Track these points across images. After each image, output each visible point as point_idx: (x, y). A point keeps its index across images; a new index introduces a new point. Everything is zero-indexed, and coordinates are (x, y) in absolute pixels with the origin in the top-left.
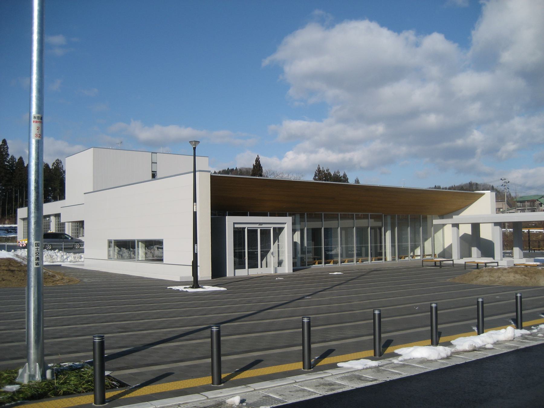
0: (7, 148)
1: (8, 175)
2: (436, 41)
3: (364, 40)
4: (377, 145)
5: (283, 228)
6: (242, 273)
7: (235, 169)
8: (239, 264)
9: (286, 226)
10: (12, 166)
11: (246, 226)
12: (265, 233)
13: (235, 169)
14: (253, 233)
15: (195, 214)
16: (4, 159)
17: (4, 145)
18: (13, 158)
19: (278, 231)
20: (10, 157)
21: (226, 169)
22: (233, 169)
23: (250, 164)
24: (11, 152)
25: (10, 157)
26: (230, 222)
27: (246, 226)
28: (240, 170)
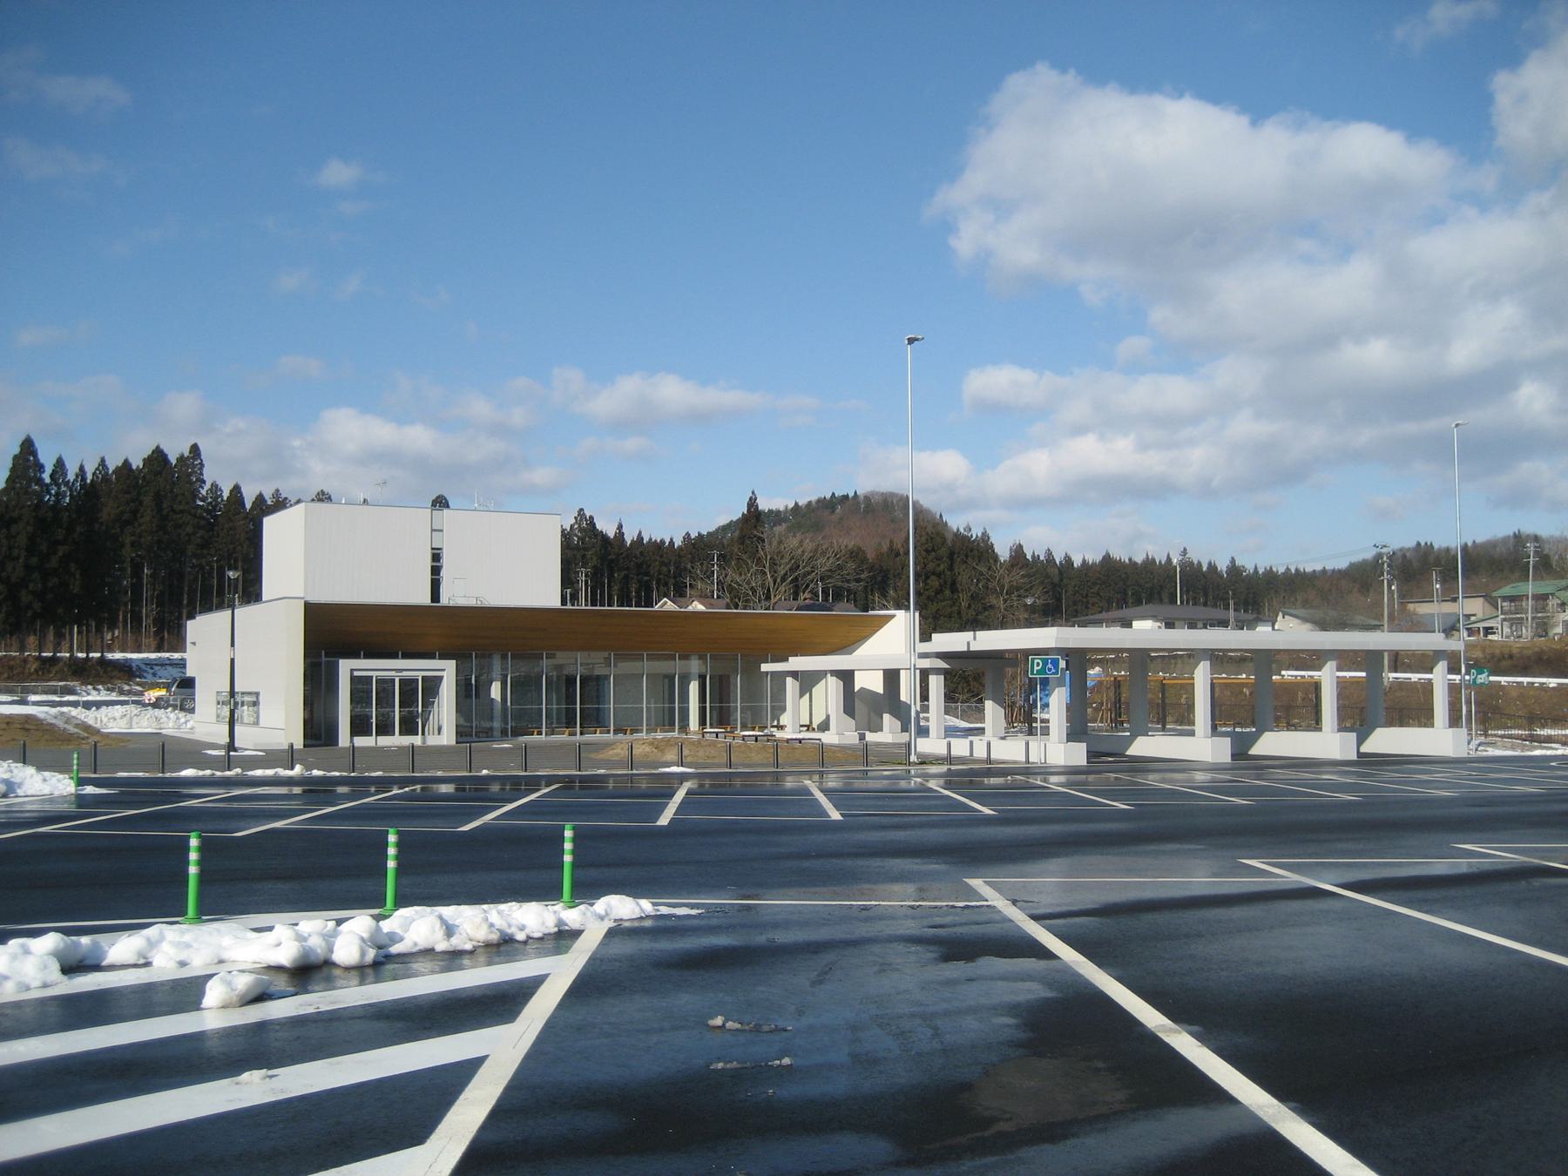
0: (202, 465)
1: (201, 533)
2: (1366, 148)
3: (1173, 142)
4: (1245, 427)
5: (441, 678)
6: (360, 741)
7: (851, 494)
8: (360, 726)
9: (444, 674)
10: (214, 508)
11: (374, 674)
12: (408, 686)
13: (851, 494)
14: (385, 685)
15: (232, 661)
16: (195, 494)
17: (194, 458)
18: (215, 488)
19: (432, 685)
20: (207, 486)
21: (828, 496)
22: (846, 497)
23: (738, 510)
24: (210, 475)
25: (207, 486)
26: (346, 667)
27: (374, 674)
28: (867, 498)
